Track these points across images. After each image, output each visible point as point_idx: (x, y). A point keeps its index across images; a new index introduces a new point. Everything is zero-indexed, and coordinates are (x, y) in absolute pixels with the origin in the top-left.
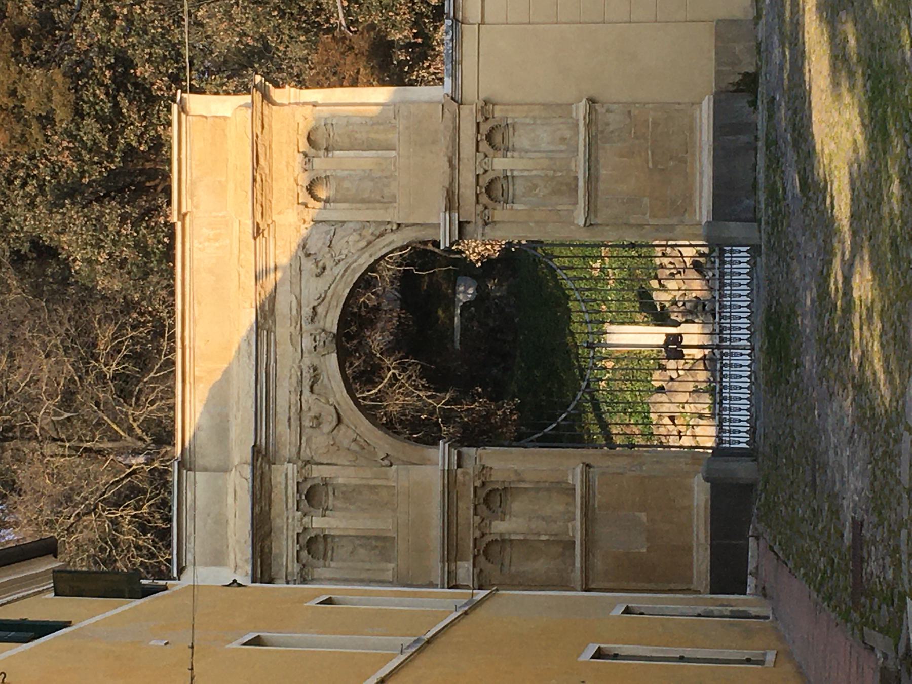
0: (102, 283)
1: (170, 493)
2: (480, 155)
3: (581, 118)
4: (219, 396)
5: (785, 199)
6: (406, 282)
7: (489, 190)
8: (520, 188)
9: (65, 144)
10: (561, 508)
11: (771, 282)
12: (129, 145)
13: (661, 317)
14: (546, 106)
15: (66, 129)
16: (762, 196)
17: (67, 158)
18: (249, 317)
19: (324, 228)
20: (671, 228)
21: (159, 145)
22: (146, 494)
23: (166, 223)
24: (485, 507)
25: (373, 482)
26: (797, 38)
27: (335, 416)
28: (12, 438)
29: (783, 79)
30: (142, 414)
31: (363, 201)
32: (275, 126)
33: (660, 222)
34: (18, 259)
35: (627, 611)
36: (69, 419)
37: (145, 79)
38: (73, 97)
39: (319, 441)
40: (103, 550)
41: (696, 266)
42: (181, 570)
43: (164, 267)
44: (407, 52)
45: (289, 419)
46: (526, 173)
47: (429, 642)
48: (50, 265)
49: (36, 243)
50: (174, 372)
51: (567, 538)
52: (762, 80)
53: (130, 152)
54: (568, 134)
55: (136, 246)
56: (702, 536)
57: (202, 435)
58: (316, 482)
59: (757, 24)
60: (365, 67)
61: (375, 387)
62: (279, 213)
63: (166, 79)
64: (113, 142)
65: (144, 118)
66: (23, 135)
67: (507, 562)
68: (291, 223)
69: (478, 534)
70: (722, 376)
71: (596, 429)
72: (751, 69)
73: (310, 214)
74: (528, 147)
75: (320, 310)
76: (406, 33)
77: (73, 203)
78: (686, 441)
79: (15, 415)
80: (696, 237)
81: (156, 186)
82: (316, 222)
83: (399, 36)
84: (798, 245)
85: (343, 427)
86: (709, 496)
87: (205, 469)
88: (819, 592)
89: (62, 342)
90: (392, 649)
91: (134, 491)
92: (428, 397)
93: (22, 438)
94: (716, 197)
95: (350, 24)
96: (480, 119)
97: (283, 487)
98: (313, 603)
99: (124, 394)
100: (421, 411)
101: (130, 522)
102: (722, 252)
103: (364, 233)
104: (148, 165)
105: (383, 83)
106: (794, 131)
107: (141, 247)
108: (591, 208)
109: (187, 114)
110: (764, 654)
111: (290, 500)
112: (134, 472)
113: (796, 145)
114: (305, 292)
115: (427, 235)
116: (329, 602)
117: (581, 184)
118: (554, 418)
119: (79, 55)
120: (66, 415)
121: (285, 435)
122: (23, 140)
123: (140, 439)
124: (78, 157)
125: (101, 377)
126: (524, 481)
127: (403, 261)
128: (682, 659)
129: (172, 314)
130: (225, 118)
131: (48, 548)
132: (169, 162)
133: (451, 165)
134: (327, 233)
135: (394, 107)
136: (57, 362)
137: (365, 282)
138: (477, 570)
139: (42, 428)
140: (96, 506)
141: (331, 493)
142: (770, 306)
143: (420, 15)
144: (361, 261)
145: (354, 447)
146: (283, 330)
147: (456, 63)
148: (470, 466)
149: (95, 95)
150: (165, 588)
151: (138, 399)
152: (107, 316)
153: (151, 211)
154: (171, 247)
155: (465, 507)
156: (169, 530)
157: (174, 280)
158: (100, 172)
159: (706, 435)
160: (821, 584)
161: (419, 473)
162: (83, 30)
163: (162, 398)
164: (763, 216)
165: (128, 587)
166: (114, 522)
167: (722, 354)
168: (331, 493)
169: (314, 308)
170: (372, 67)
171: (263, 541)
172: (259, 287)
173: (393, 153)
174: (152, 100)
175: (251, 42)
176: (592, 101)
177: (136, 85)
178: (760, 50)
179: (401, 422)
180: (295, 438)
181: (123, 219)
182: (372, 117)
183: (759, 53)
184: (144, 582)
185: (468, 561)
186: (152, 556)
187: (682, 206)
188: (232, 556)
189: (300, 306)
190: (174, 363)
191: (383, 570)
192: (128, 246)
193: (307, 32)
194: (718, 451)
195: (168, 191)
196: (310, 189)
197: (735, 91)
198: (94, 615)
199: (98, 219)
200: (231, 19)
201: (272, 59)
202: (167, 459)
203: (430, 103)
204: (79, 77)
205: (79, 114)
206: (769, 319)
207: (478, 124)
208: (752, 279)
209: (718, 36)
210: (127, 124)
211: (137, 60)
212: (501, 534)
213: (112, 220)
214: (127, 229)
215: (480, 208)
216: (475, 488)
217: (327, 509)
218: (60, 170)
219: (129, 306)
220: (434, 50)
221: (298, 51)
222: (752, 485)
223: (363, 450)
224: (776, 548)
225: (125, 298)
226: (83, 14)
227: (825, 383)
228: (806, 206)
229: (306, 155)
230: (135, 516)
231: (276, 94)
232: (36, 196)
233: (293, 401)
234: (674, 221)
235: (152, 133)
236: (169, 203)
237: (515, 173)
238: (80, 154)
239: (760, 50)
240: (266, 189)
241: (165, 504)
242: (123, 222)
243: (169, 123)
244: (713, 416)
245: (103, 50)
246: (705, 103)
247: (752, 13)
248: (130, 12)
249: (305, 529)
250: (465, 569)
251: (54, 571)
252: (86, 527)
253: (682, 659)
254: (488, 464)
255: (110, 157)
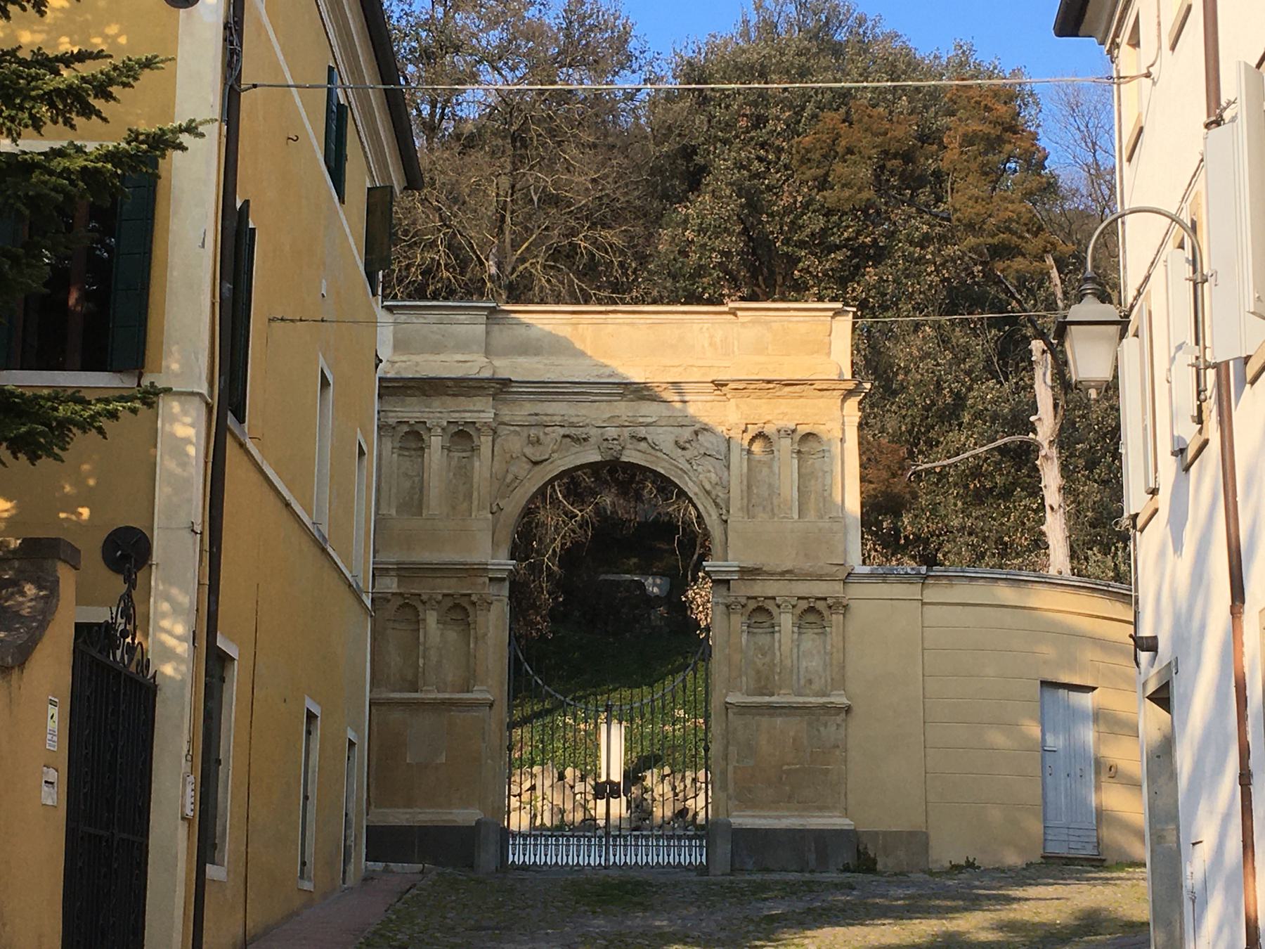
0: (666, 233)
1: (461, 299)
2: (794, 601)
3: (832, 700)
4: (560, 347)
5: (757, 900)
6: (665, 528)
7: (760, 609)
8: (763, 640)
9: (800, 199)
10: (450, 678)
11: (675, 886)
12: (799, 260)
13: (633, 775)
14: (843, 667)
15: (814, 199)
16: (757, 877)
17: (786, 200)
18: (637, 376)
19: (723, 449)
20: (724, 788)
21: (797, 290)
22: (462, 274)
23: (724, 295)
24: (451, 604)
25: (475, 494)
26: (915, 912)
27: (539, 459)
28: (514, 147)
29: (874, 897)
30: (538, 271)
31: (749, 487)
32: (821, 403)
33: (730, 775)
34: (688, 153)
35: (351, 744)
36: (532, 200)
37: (863, 275)
38: (847, 207)
39: (515, 444)
40: (406, 232)
41: (683, 813)
42: (390, 309)
43: (681, 292)
44: (890, 529)
45: (536, 415)
46: (777, 645)
47: (324, 550)
48: (682, 183)
49: (704, 170)
50: (578, 303)
51: (421, 683)
52: (870, 877)
53: (793, 261)
54: (816, 687)
55: (701, 266)
56: (421, 817)
57: (521, 330)
58: (475, 439)
59: (924, 872)
60: (874, 489)
61: (564, 497)
62: (737, 406)
63: (864, 295)
64: (801, 244)
65: (825, 274)
66: (809, 160)
67: (397, 626)
68: (728, 417)
69: (424, 597)
70: (579, 838)
71: (528, 710)
72: (879, 867)
73: (736, 434)
74: (802, 649)
75: (643, 445)
76: (909, 528)
77: (742, 206)
78: (514, 802)
79: (537, 148)
80: (715, 810)
81: (759, 287)
82: (729, 440)
83: (906, 521)
84: (712, 913)
85: (528, 466)
86: (461, 823)
87: (487, 333)
88: (375, 933)
89: (607, 195)
90: (316, 512)
91: (463, 265)
92: (554, 550)
93: (514, 156)
94: (754, 831)
95: (917, 474)
96: (830, 601)
97: (472, 408)
98: (359, 436)
99: (556, 254)
100: (540, 542)
101: (433, 259)
102: (700, 838)
103: (719, 488)
104: (780, 279)
105: (863, 505)
106: (824, 909)
107: (700, 271)
108: (744, 709)
109: (833, 317)
110: (310, 879)
111: (457, 415)
112: (482, 263)
113: (809, 911)
114: (660, 430)
115: (717, 547)
116: (361, 453)
117: (767, 699)
118: (538, 672)
119: (886, 212)
120: (535, 199)
121: (521, 411)
122: (805, 161)
123: (514, 269)
124: (788, 210)
125: (573, 233)
126: (476, 643)
127: (687, 524)
128: (306, 798)
129: (635, 301)
130: (829, 354)
131: (413, 180)
132: (783, 300)
133: (783, 573)
134: (718, 452)
135: (840, 518)
136: (587, 189)
137: (666, 486)
138: (389, 596)
139: (524, 174)
140: (449, 227)
141: (464, 454)
142: (650, 885)
143: (926, 542)
144: (690, 484)
145: (510, 477)
146: (623, 409)
147: (884, 578)
148: (493, 590)
149: (848, 227)
150: (375, 294)
151: (552, 267)
152: (632, 238)
153: (734, 281)
154: (699, 301)
155: (450, 586)
156: (424, 298)
157: (668, 304)
158: (772, 233)
159: (518, 821)
160: (382, 936)
161: (485, 540)
162: (910, 217)
163: (552, 291)
164: (739, 877)
165: (377, 256)
166: (433, 244)
167: (600, 838)
168: (464, 454)
169: (645, 439)
170: (876, 496)
171: (418, 388)
172: (664, 386)
173: (796, 516)
174: (843, 282)
175: (900, 377)
176: (848, 710)
177: (857, 267)
178: (900, 876)
179: (530, 523)
180: (518, 419)
181: (727, 254)
182: (831, 495)
183: (896, 874)
184: (381, 273)
185: (399, 587)
186: (400, 282)
187: (746, 800)
188: (404, 358)
189: (648, 425)
190: (586, 302)
191: (389, 505)
192: (700, 258)
193: (910, 432)
194: (506, 833)
195: (753, 298)
196: (761, 435)
197: (858, 851)
198: (349, 226)
199: (726, 230)
200: (922, 359)
201: (883, 398)
202: (495, 296)
203: (845, 552)
204: (865, 212)
205: (829, 213)
206: (638, 884)
207: (825, 599)
208: (674, 867)
209: (912, 834)
210: (819, 258)
211: (881, 267)
212: (424, 620)
213: (725, 243)
214: (716, 258)
215: (743, 601)
216: (470, 595)
217: (450, 451)
218: (776, 194)
219: (643, 259)
220: (893, 555)
221: (891, 424)
222: (471, 866)
223: (506, 486)
224: (414, 891)
225: (650, 255)
226: (926, 216)
227: (579, 940)
228: (752, 920)
229: (794, 431)
230: (439, 264)
231: (853, 403)
232: (749, 171)
233: (555, 418)
234: (731, 791)
235: (811, 283)
236: (742, 299)
237: (777, 635)
238: (792, 212)
239: (900, 876)
240: (759, 393)
241: (450, 294)
242: (723, 254)
243: (821, 299)
244: (535, 828)
245: (891, 235)
246: (848, 821)
247: (935, 867)
248: (928, 262)
249: (430, 430)
250: (391, 585)
251: (392, 187)
252: (428, 217)
253: (306, 798)
254: (492, 607)
255: (787, 242)
